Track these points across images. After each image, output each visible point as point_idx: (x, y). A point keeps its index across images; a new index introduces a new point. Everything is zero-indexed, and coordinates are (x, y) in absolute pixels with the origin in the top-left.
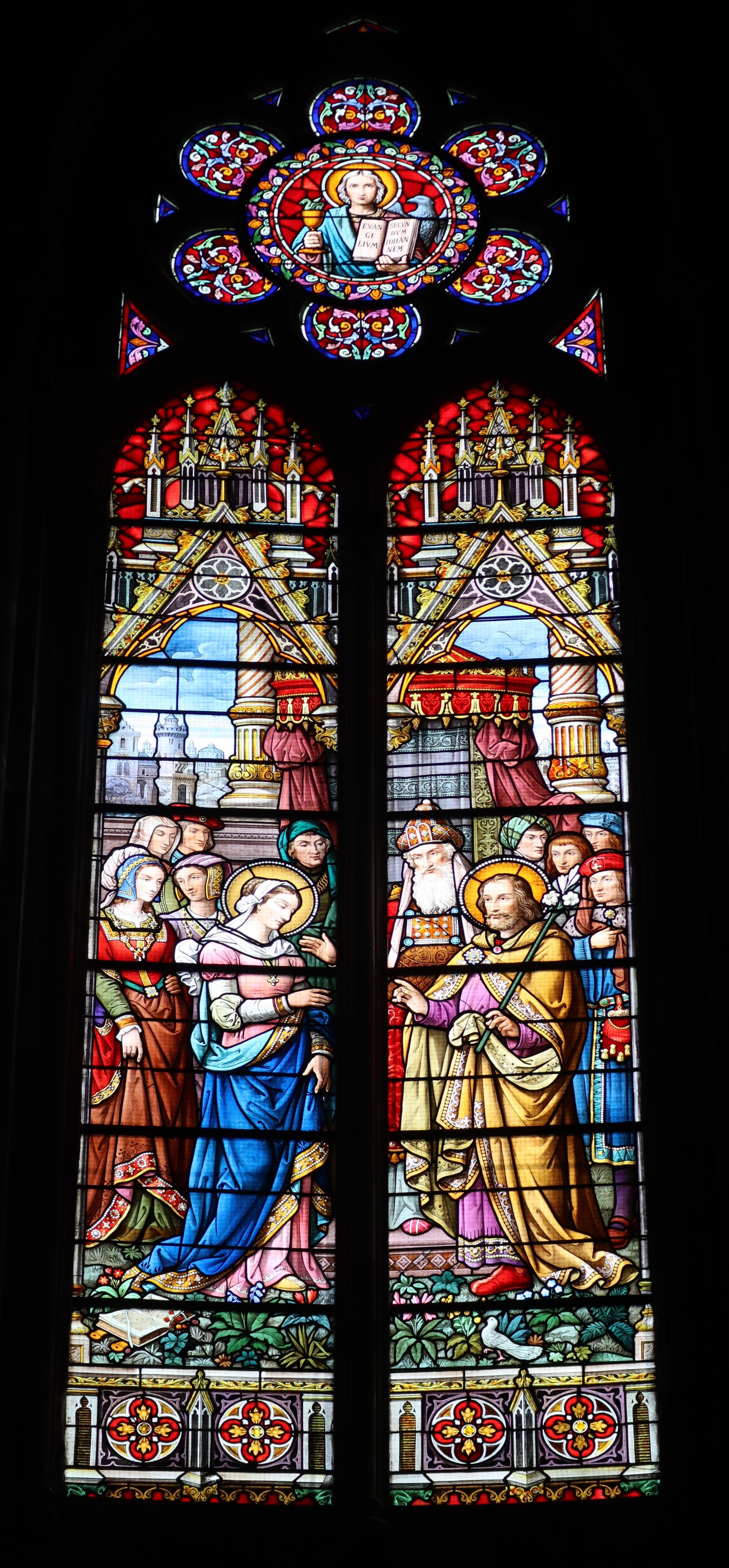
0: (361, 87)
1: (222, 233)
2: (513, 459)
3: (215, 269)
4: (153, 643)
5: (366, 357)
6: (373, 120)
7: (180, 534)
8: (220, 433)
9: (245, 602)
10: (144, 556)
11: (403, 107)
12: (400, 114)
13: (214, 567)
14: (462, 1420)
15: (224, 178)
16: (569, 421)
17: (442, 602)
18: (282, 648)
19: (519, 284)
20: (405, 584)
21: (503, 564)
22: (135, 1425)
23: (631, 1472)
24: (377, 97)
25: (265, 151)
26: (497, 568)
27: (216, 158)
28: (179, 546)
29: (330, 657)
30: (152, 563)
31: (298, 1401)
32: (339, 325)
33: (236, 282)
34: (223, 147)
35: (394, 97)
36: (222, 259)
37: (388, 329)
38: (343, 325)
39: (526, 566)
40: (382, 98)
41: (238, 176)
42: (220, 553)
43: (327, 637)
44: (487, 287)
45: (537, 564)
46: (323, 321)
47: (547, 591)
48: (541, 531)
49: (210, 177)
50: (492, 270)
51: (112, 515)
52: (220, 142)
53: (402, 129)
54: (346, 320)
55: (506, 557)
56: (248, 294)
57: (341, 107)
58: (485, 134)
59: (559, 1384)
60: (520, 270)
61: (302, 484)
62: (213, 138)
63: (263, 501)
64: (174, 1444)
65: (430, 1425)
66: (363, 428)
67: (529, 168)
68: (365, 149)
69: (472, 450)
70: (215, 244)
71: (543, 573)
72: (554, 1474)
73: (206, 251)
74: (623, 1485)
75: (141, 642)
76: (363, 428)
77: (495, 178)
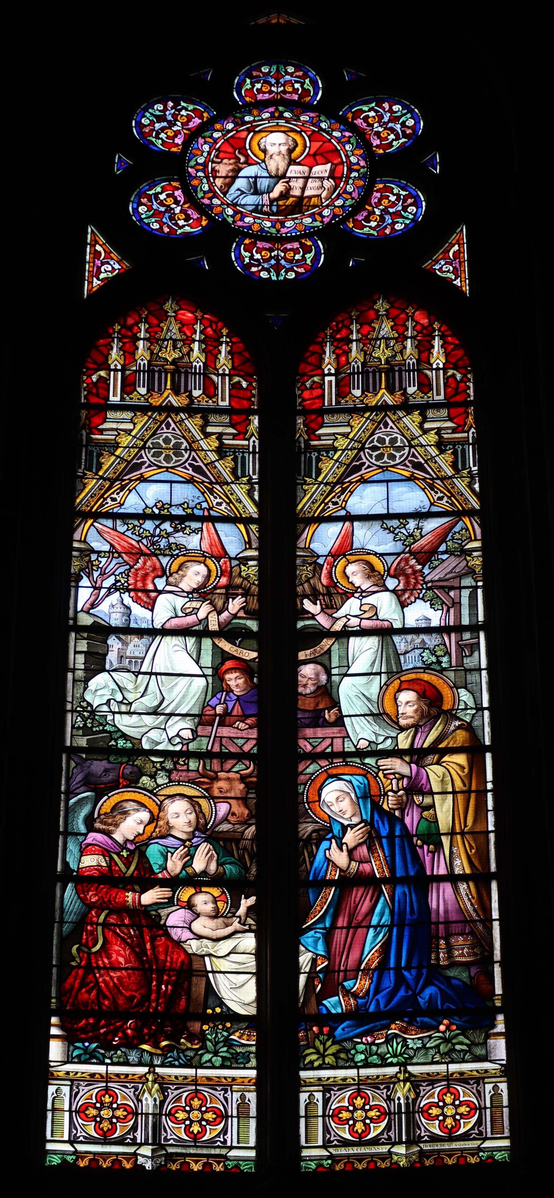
2: (394, 356)
4: (114, 500)
5: (281, 278)
6: (284, 92)
7: (135, 415)
8: (168, 338)
9: (185, 468)
10: (107, 433)
13: (161, 441)
14: (191, 1106)
15: (168, 137)
16: (225, 331)
17: (338, 468)
18: (214, 503)
19: (398, 222)
20: (310, 453)
21: (167, 441)
22: (442, 1108)
23: (488, 1144)
24: (287, 73)
26: (387, 442)
27: (164, 124)
28: (135, 424)
29: (252, 510)
30: (114, 437)
31: (229, 1092)
32: (261, 253)
33: (179, 219)
39: (185, 444)
40: (291, 75)
41: (179, 136)
42: (165, 430)
43: (250, 494)
45: (413, 439)
46: (306, 92)
47: (201, 464)
48: (417, 413)
49: (157, 137)
50: (378, 212)
51: (83, 401)
53: (308, 99)
54: (266, 249)
55: (169, 435)
56: (188, 229)
57: (298, 261)
58: (373, 105)
59: (478, 1075)
60: (158, 122)
61: (231, 376)
62: (160, 107)
63: (414, 386)
64: (383, 1124)
65: (419, 1107)
66: (280, 334)
67: (409, 131)
68: (267, 115)
69: (362, 350)
70: (164, 190)
71: (418, 445)
72: (81, 1148)
73: (156, 195)
74: (481, 1154)
75: (327, 504)
76: (280, 334)
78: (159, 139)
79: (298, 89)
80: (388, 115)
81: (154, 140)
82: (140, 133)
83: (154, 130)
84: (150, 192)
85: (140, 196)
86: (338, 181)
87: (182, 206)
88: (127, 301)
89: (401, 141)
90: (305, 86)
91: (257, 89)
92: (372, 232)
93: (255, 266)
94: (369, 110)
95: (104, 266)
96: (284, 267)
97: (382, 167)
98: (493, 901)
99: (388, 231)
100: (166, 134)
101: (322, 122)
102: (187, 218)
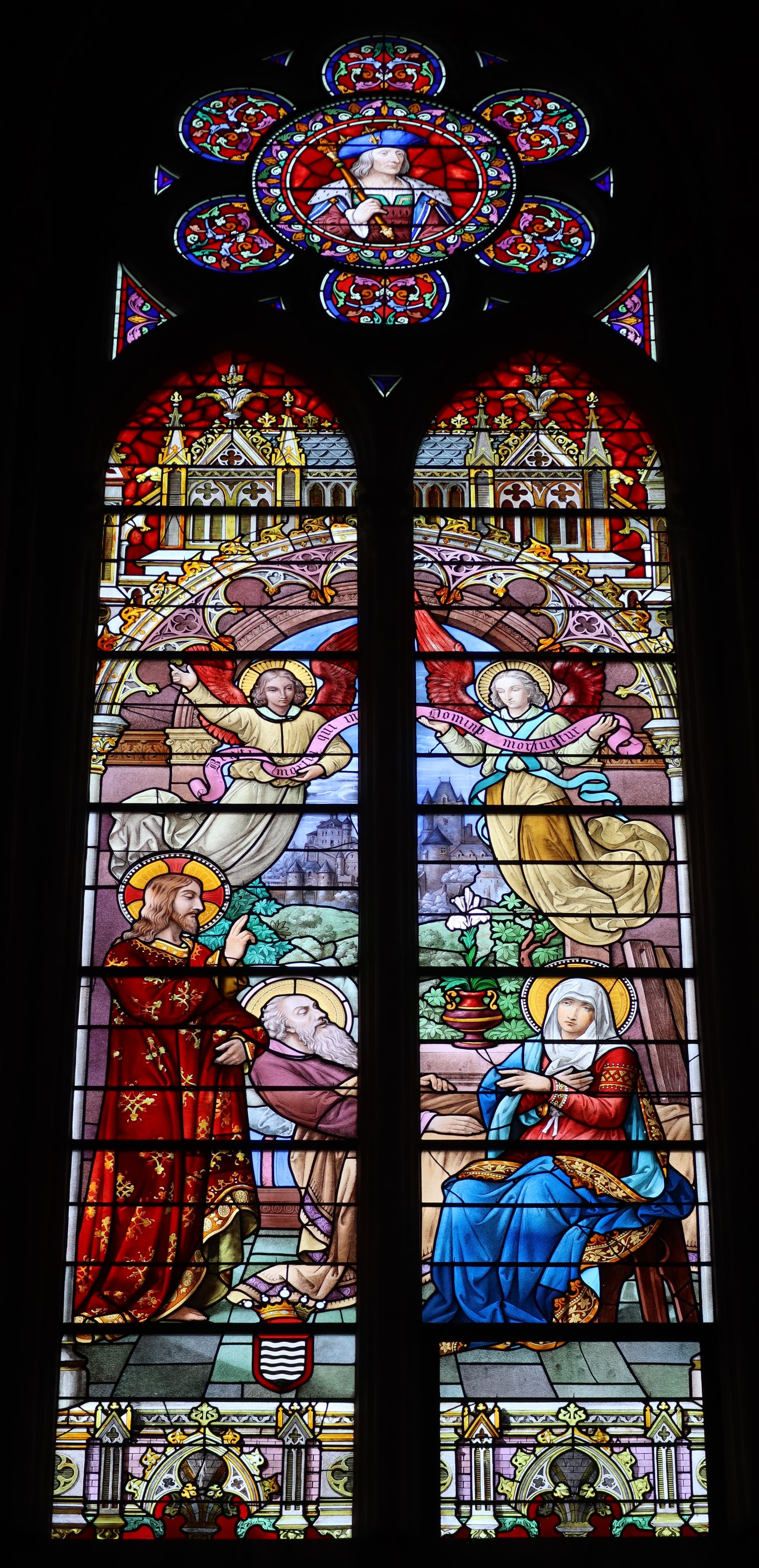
0: (379, 45)
1: (231, 200)
3: (220, 237)
6: (375, 288)
11: (425, 65)
12: (343, 295)
19: (557, 256)
24: (371, 315)
25: (275, 115)
33: (521, 115)
34: (229, 112)
35: (415, 55)
40: (365, 313)
44: (523, 255)
46: (425, 80)
49: (558, 221)
52: (549, 259)
54: (368, 287)
56: (255, 262)
58: (521, 99)
60: (214, 124)
68: (371, 112)
73: (212, 220)
76: (382, 388)
77: (532, 144)
78: (217, 145)
79: (412, 76)
80: (540, 113)
81: (562, 217)
82: (582, 226)
83: (209, 134)
84: (204, 217)
85: (191, 220)
86: (463, 197)
88: (179, 364)
89: (207, 215)
91: (415, 292)
93: (353, 309)
94: (249, 260)
95: (133, 319)
96: (394, 310)
97: (233, 179)
101: (318, 243)
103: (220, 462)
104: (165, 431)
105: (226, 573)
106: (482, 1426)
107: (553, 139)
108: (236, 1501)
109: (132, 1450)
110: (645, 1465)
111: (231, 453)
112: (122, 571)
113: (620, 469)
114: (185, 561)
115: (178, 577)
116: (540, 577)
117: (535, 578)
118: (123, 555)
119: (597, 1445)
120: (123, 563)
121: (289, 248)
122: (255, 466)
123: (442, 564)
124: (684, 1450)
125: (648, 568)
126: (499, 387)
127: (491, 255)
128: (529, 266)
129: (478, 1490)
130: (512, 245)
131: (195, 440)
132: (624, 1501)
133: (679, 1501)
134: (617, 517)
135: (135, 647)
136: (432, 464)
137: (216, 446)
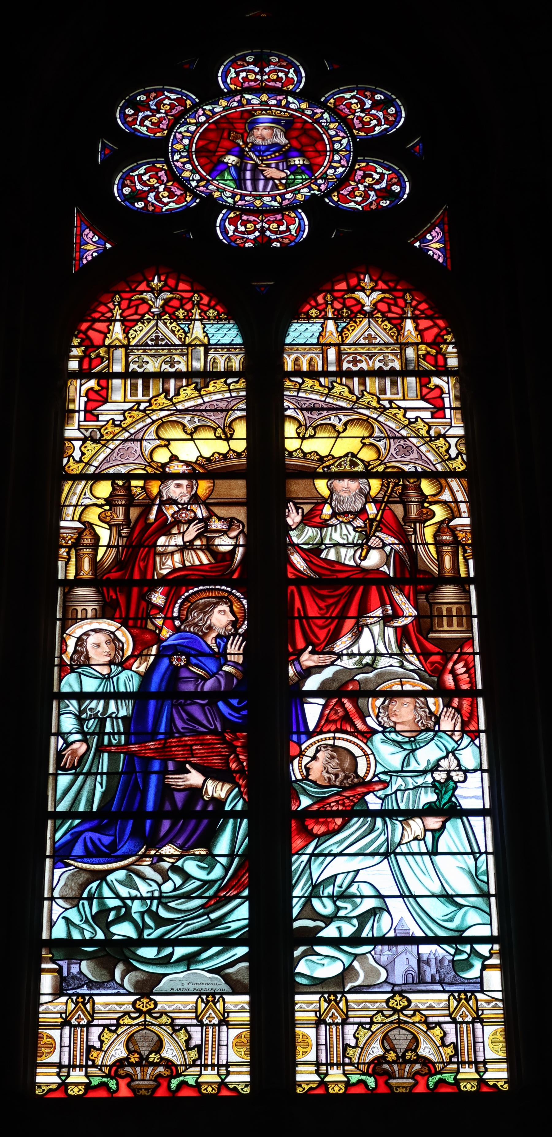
11: (291, 71)
15: (371, 176)
33: (356, 104)
34: (151, 103)
35: (284, 64)
36: (153, 181)
37: (283, 228)
38: (275, 77)
46: (290, 81)
49: (142, 124)
50: (361, 187)
53: (232, 215)
56: (173, 205)
57: (282, 232)
58: (355, 93)
66: (262, 291)
70: (373, 129)
76: (262, 291)
78: (144, 126)
80: (370, 102)
81: (384, 171)
82: (400, 177)
87: (165, 184)
88: (116, 275)
90: (290, 76)
92: (357, 207)
95: (91, 246)
97: (156, 149)
98: (434, 647)
99: (373, 207)
100: (374, 179)
102: (171, 195)
103: (150, 343)
104: (111, 321)
105: (154, 417)
106: (464, 1009)
107: (379, 120)
108: (169, 1064)
109: (347, 1027)
110: (451, 1038)
111: (157, 337)
112: (82, 419)
113: (429, 345)
114: (125, 411)
115: (121, 421)
116: (369, 417)
117: (365, 418)
118: (82, 407)
119: (159, 1025)
120: (82, 414)
121: (195, 196)
122: (175, 345)
123: (302, 409)
124: (224, 1029)
125: (447, 411)
126: (134, 291)
127: (336, 199)
128: (363, 207)
129: (75, 1058)
130: (350, 192)
131: (131, 328)
132: (181, 1065)
133: (476, 1063)
134: (423, 376)
135: (91, 470)
136: (294, 342)
137: (141, 333)
